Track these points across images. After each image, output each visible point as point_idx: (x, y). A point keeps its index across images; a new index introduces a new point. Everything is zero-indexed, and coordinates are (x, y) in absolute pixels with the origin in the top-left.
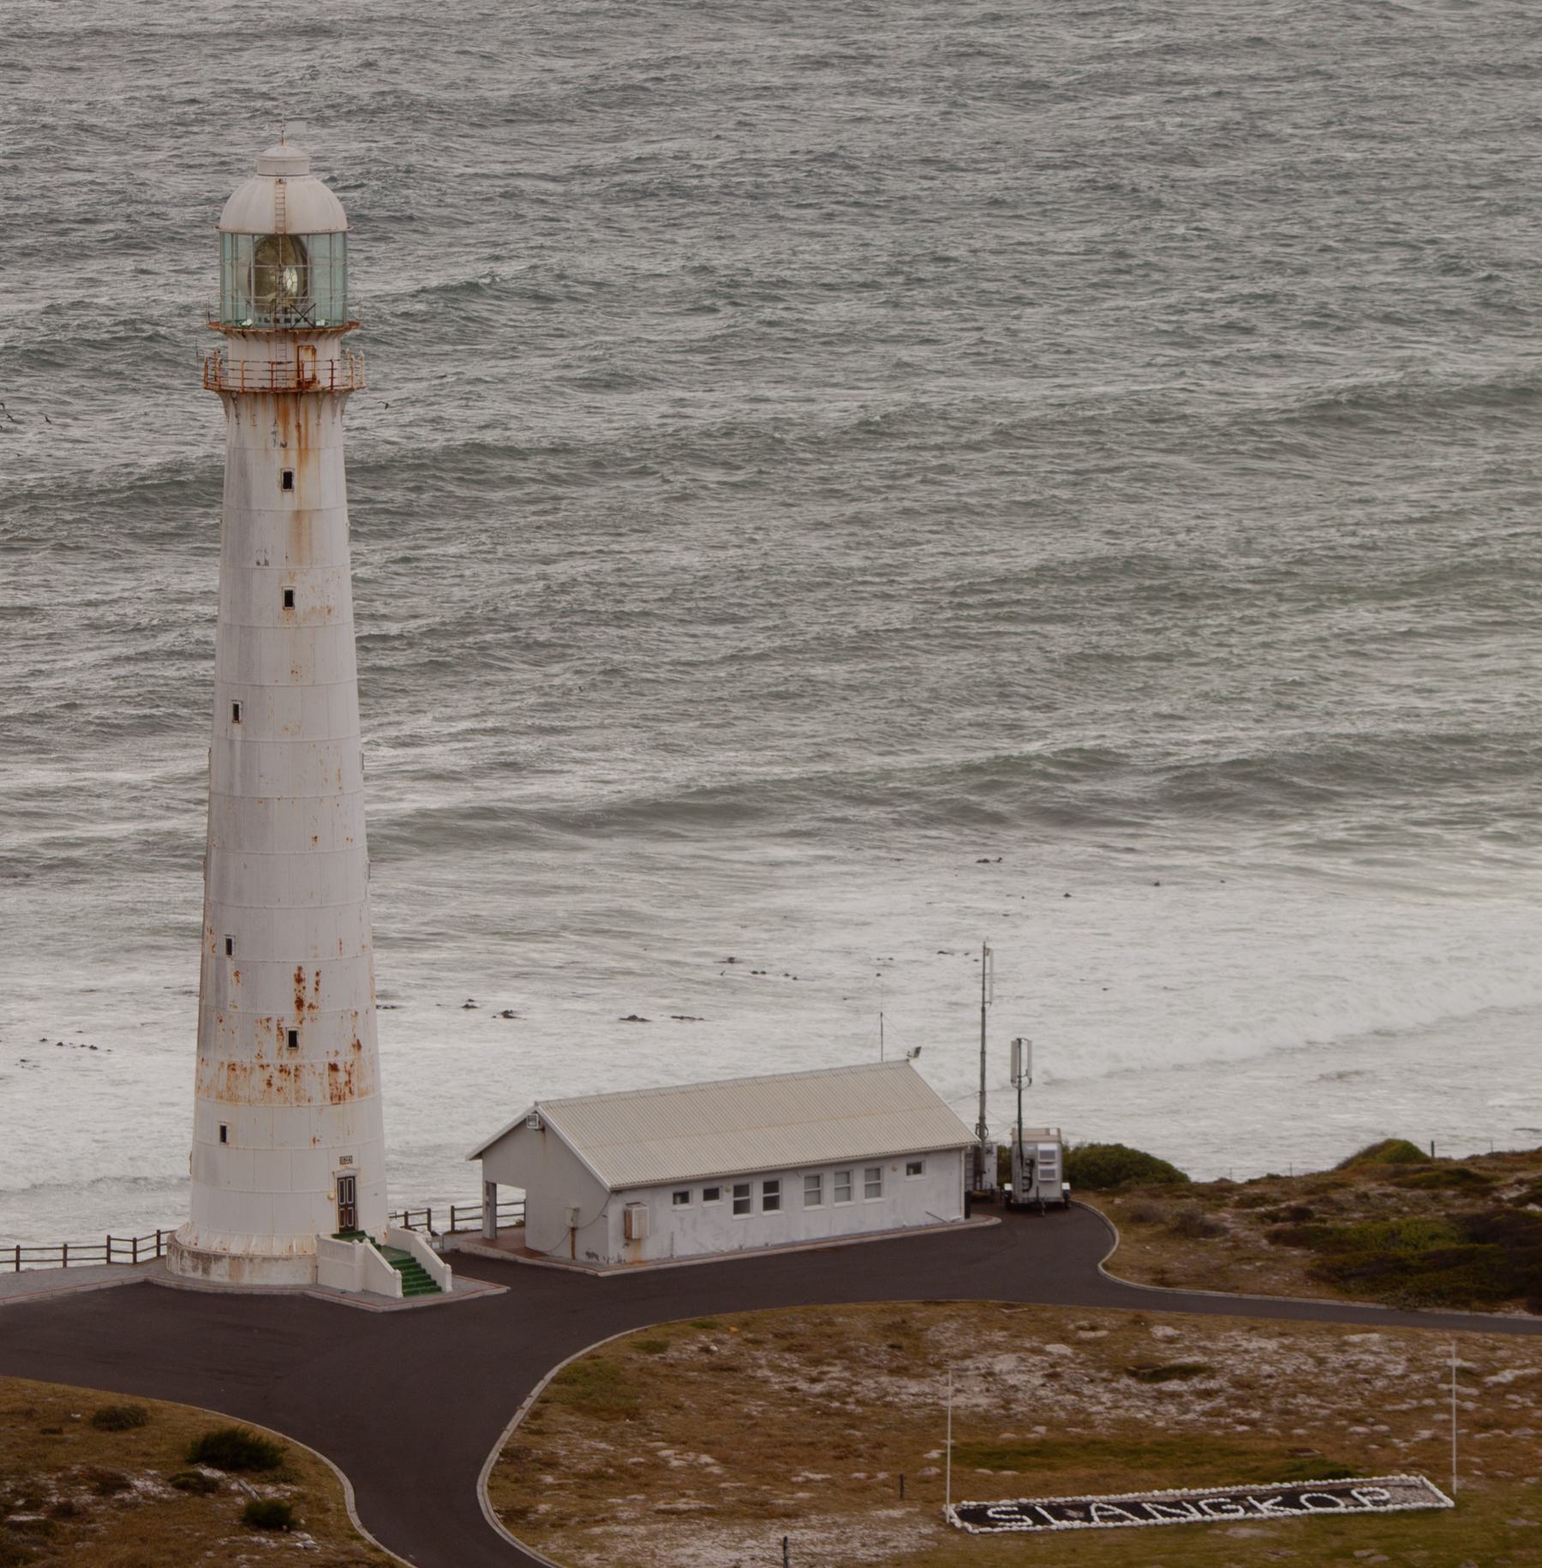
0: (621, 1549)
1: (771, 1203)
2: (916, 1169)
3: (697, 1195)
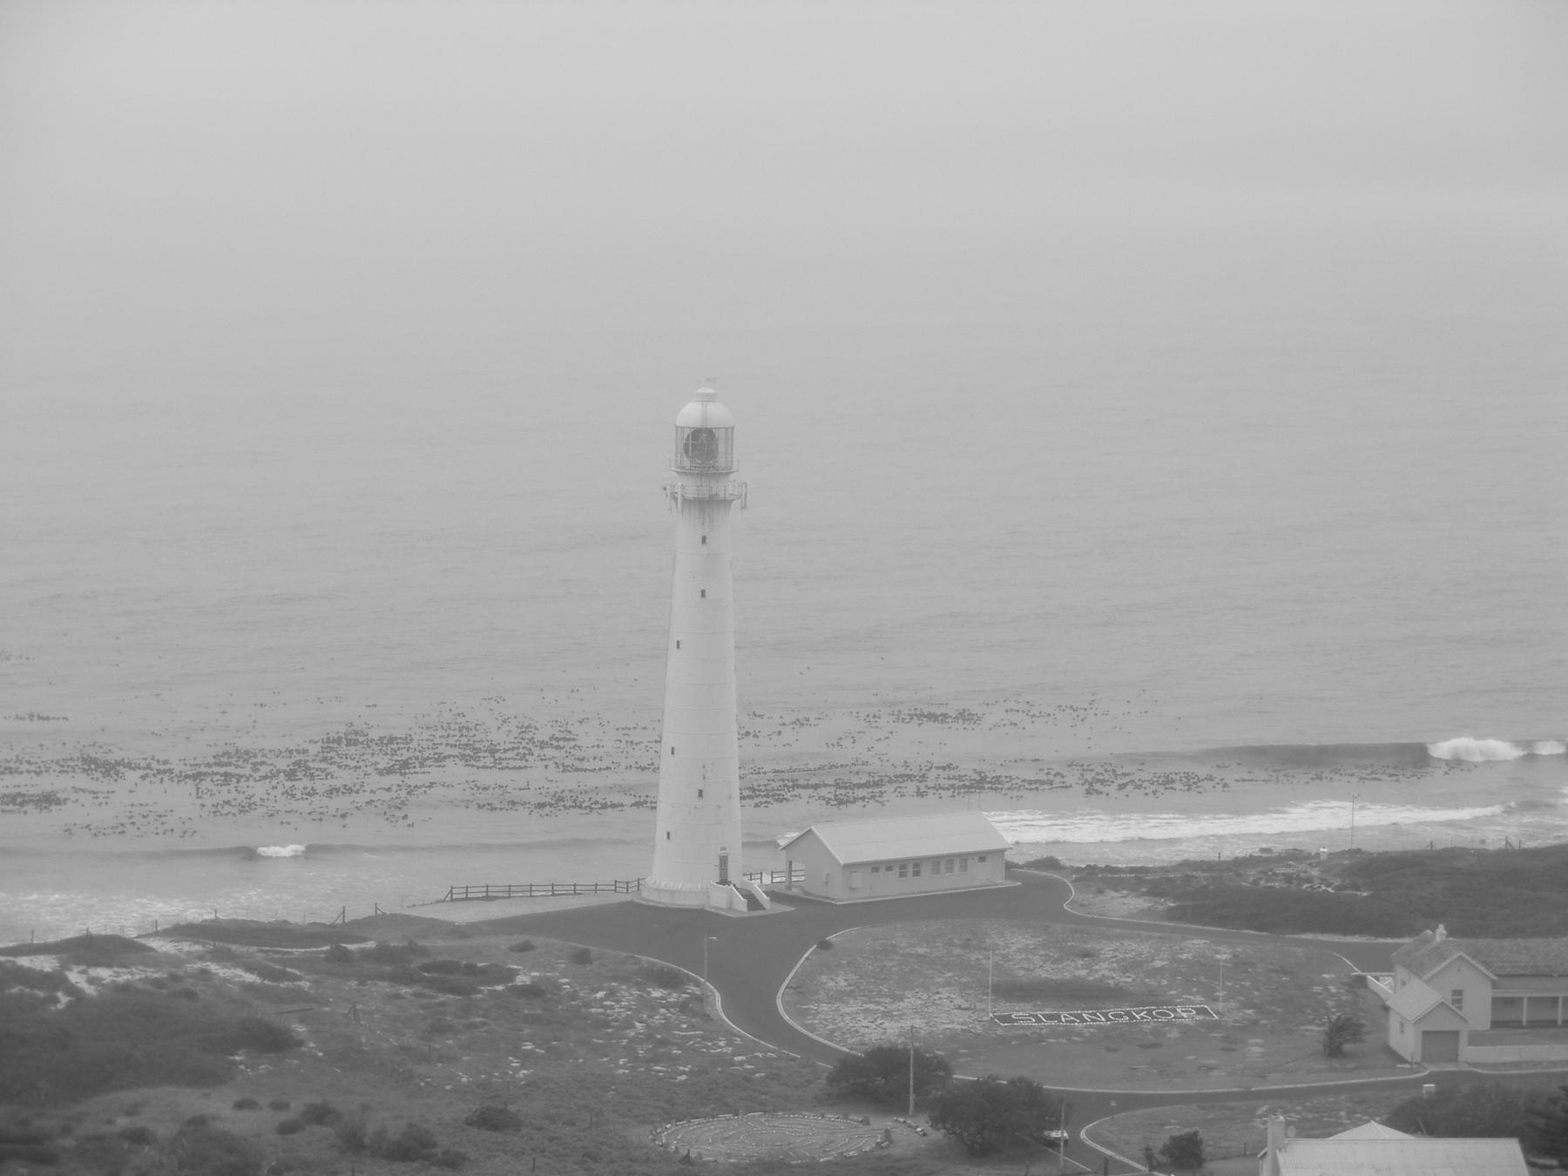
1: (916, 873)
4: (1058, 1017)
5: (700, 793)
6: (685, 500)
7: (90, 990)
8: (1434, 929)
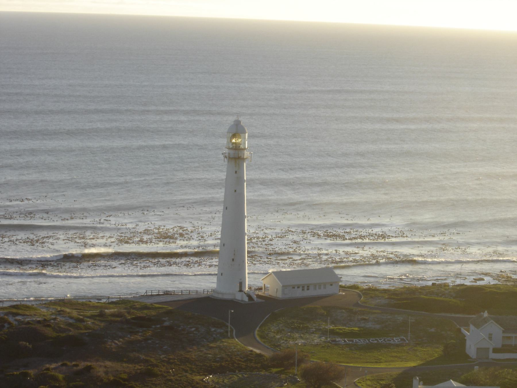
0: (291, 342)
1: (308, 289)
2: (332, 285)
3: (296, 288)
4: (353, 341)
5: (233, 260)
6: (229, 158)
7: (15, 323)
8: (484, 312)
